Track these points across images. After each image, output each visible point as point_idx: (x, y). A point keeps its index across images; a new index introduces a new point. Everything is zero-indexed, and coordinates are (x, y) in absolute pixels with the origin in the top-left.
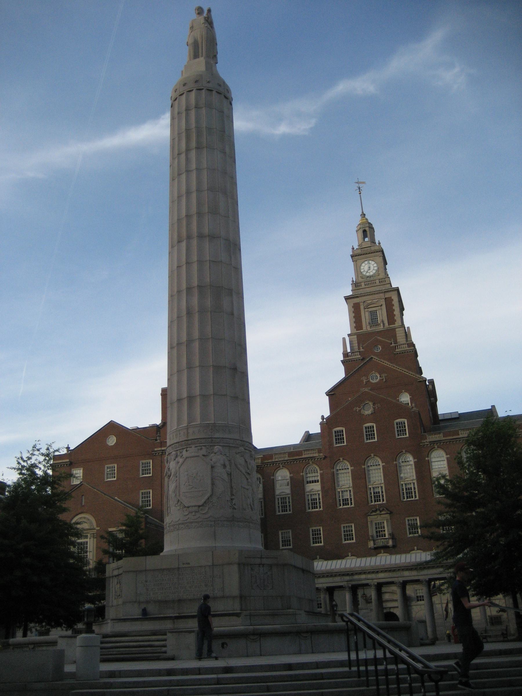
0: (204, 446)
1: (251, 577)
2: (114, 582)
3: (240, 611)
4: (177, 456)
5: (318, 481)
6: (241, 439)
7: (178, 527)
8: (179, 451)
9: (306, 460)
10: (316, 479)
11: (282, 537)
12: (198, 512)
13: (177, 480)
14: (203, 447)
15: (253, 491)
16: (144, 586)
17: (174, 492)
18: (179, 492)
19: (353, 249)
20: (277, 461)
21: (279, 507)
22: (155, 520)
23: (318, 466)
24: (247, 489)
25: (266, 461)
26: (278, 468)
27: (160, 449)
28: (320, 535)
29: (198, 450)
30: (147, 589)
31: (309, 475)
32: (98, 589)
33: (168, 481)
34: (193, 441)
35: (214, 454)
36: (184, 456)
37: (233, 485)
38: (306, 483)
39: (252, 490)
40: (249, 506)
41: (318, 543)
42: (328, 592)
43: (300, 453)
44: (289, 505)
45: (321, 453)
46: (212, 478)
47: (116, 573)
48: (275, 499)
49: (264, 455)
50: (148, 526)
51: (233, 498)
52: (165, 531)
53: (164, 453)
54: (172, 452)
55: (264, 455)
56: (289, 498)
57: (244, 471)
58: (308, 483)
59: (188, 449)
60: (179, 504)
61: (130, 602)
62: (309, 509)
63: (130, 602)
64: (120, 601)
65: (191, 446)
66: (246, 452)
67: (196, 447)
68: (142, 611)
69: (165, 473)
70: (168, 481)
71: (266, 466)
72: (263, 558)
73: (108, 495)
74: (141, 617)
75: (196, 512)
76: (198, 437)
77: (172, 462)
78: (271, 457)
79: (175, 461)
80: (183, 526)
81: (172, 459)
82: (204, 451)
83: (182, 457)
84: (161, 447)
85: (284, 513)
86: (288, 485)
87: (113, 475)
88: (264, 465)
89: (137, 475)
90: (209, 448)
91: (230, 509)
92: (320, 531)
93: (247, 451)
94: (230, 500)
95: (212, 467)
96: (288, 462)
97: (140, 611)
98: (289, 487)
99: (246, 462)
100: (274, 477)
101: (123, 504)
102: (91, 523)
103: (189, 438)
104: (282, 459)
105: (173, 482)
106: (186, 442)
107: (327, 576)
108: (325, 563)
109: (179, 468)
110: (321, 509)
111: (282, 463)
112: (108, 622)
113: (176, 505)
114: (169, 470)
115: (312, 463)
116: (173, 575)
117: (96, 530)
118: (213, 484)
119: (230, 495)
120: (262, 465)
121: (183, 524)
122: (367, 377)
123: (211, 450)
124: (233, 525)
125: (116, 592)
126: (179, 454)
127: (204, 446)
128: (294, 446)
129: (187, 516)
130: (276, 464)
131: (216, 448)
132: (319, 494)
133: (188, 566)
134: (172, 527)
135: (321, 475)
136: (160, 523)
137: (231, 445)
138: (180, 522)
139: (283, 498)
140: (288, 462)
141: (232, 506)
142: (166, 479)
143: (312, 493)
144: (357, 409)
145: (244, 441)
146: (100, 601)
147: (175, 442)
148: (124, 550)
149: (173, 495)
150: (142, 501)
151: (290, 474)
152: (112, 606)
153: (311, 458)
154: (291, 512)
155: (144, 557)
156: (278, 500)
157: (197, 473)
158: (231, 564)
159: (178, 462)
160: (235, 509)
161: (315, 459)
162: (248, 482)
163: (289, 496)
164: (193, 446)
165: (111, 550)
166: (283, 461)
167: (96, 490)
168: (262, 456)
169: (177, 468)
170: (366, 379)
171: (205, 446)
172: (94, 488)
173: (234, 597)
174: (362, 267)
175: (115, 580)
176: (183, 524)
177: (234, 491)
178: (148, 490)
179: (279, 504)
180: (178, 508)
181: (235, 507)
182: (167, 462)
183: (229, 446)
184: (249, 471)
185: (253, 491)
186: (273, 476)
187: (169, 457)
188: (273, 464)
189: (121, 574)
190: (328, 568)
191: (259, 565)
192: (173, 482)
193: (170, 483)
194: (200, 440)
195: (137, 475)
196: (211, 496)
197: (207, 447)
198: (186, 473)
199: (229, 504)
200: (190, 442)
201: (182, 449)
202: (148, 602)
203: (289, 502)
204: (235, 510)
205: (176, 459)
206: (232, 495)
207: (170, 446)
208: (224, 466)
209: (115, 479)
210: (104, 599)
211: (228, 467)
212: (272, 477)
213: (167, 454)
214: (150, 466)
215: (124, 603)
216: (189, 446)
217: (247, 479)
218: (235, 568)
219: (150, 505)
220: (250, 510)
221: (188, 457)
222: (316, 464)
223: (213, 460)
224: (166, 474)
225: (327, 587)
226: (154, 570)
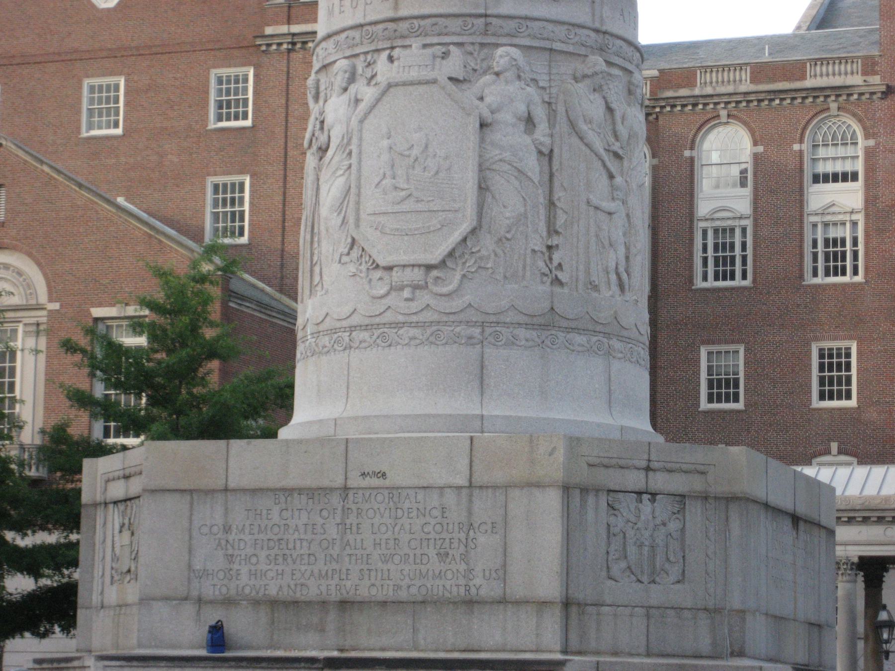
0: (454, 44)
1: (608, 537)
2: (109, 525)
3: (559, 656)
4: (352, 78)
5: (854, 177)
6: (597, 25)
7: (347, 339)
8: (362, 58)
9: (815, 97)
10: (848, 167)
11: (710, 368)
12: (426, 287)
13: (350, 167)
14: (452, 48)
15: (629, 222)
16: (219, 544)
17: (340, 206)
18: (358, 210)
20: (711, 96)
21: (705, 260)
22: (261, 285)
23: (860, 121)
24: (610, 214)
25: (670, 94)
26: (710, 121)
27: (284, 29)
28: (848, 368)
29: (434, 57)
30: (230, 558)
31: (822, 152)
32: (50, 526)
33: (318, 169)
34: (415, 21)
35: (494, 77)
36: (379, 78)
37: (556, 197)
38: (811, 179)
39: (628, 215)
40: (613, 277)
41: (840, 398)
42: (862, 573)
43: (797, 70)
44: (744, 259)
45: (874, 73)
46: (480, 165)
47: (117, 490)
49: (660, 71)
50: (232, 304)
51: (555, 242)
52: (300, 349)
53: (299, 46)
54: (335, 62)
55: (660, 71)
56: (744, 230)
57: (599, 146)
58: (818, 182)
59: (396, 53)
60: (355, 253)
61: (166, 599)
62: (815, 274)
63: (166, 599)
64: (132, 593)
66: (610, 75)
67: (425, 46)
68: (210, 632)
69: (308, 135)
70: (318, 169)
71: (668, 109)
72: (654, 470)
73: (89, 190)
74: (203, 653)
75: (415, 287)
76: (435, 11)
77: (334, 95)
78: (687, 77)
79: (345, 97)
80: (365, 335)
81: (336, 88)
82: (454, 64)
83: (373, 82)
84: (289, 23)
85: (721, 284)
86: (743, 184)
87: (112, 118)
88: (662, 107)
89: (197, 122)
90: (476, 54)
91: (543, 283)
92: (848, 355)
93: (616, 71)
94: (544, 250)
95: (483, 125)
96: (749, 102)
97: (202, 634)
98: (748, 191)
99: (610, 110)
100: (694, 153)
101: (146, 224)
102: (29, 286)
103: (403, 13)
104: (730, 89)
105: (334, 172)
106: (391, 26)
107: (866, 520)
108: (861, 471)
109: (361, 121)
110: (859, 278)
111: (727, 103)
112: (87, 663)
113: (345, 259)
114: (322, 128)
115: (839, 109)
116: (325, 513)
117: (44, 313)
118: (483, 188)
119: (545, 234)
120: (654, 107)
121: (366, 327)
123: (483, 60)
124: (548, 342)
125: (115, 558)
126: (360, 70)
127: (454, 44)
128: (778, 43)
129: (383, 301)
130: (705, 105)
131: (502, 56)
132: (854, 224)
133: (376, 482)
134: (327, 338)
135: (870, 154)
136: (278, 295)
137: (557, 46)
138: (356, 320)
139: (724, 230)
140: (749, 102)
141: (547, 271)
142: (311, 160)
143: (828, 218)
145: (605, 33)
146: (58, 568)
147: (350, 22)
148: (147, 395)
149: (336, 221)
150: (216, 216)
151: (755, 144)
152: (102, 607)
153: (837, 90)
154: (747, 283)
155: (222, 443)
157: (426, 147)
158: (538, 485)
159: (357, 101)
160: (561, 284)
161: (852, 95)
162: (613, 188)
163: (744, 222)
164: (416, 43)
165: (99, 390)
166: (730, 94)
167: (46, 169)
168: (655, 73)
169: (354, 122)
171: (460, 45)
172: (42, 162)
173: (542, 605)
175: (115, 517)
176: (366, 327)
177: (561, 219)
178: (236, 178)
179: (705, 249)
180: (352, 268)
181: (560, 275)
182: (317, 98)
183: (551, 50)
184: (618, 144)
185: (629, 222)
186: (692, 148)
187: (323, 79)
188: (695, 105)
189: (139, 497)
190: (871, 491)
191: (639, 493)
192: (334, 172)
193: (324, 175)
194: (441, 21)
195: (197, 122)
196: (473, 231)
197: (470, 48)
198: (385, 143)
199: (541, 264)
200: (403, 26)
202: (229, 602)
203: (744, 247)
204: (557, 289)
205: (353, 89)
206: (552, 231)
207: (329, 36)
208: (529, 122)
209: (119, 131)
210: (74, 563)
211: (542, 128)
212: (687, 153)
213: (316, 66)
214: (245, 90)
215: (145, 601)
216: (399, 42)
217: (611, 177)
218: (552, 500)
219: (242, 229)
220: (615, 288)
221: (397, 85)
222: (854, 115)
223: (488, 100)
224: (311, 141)
225: (861, 558)
226: (255, 492)
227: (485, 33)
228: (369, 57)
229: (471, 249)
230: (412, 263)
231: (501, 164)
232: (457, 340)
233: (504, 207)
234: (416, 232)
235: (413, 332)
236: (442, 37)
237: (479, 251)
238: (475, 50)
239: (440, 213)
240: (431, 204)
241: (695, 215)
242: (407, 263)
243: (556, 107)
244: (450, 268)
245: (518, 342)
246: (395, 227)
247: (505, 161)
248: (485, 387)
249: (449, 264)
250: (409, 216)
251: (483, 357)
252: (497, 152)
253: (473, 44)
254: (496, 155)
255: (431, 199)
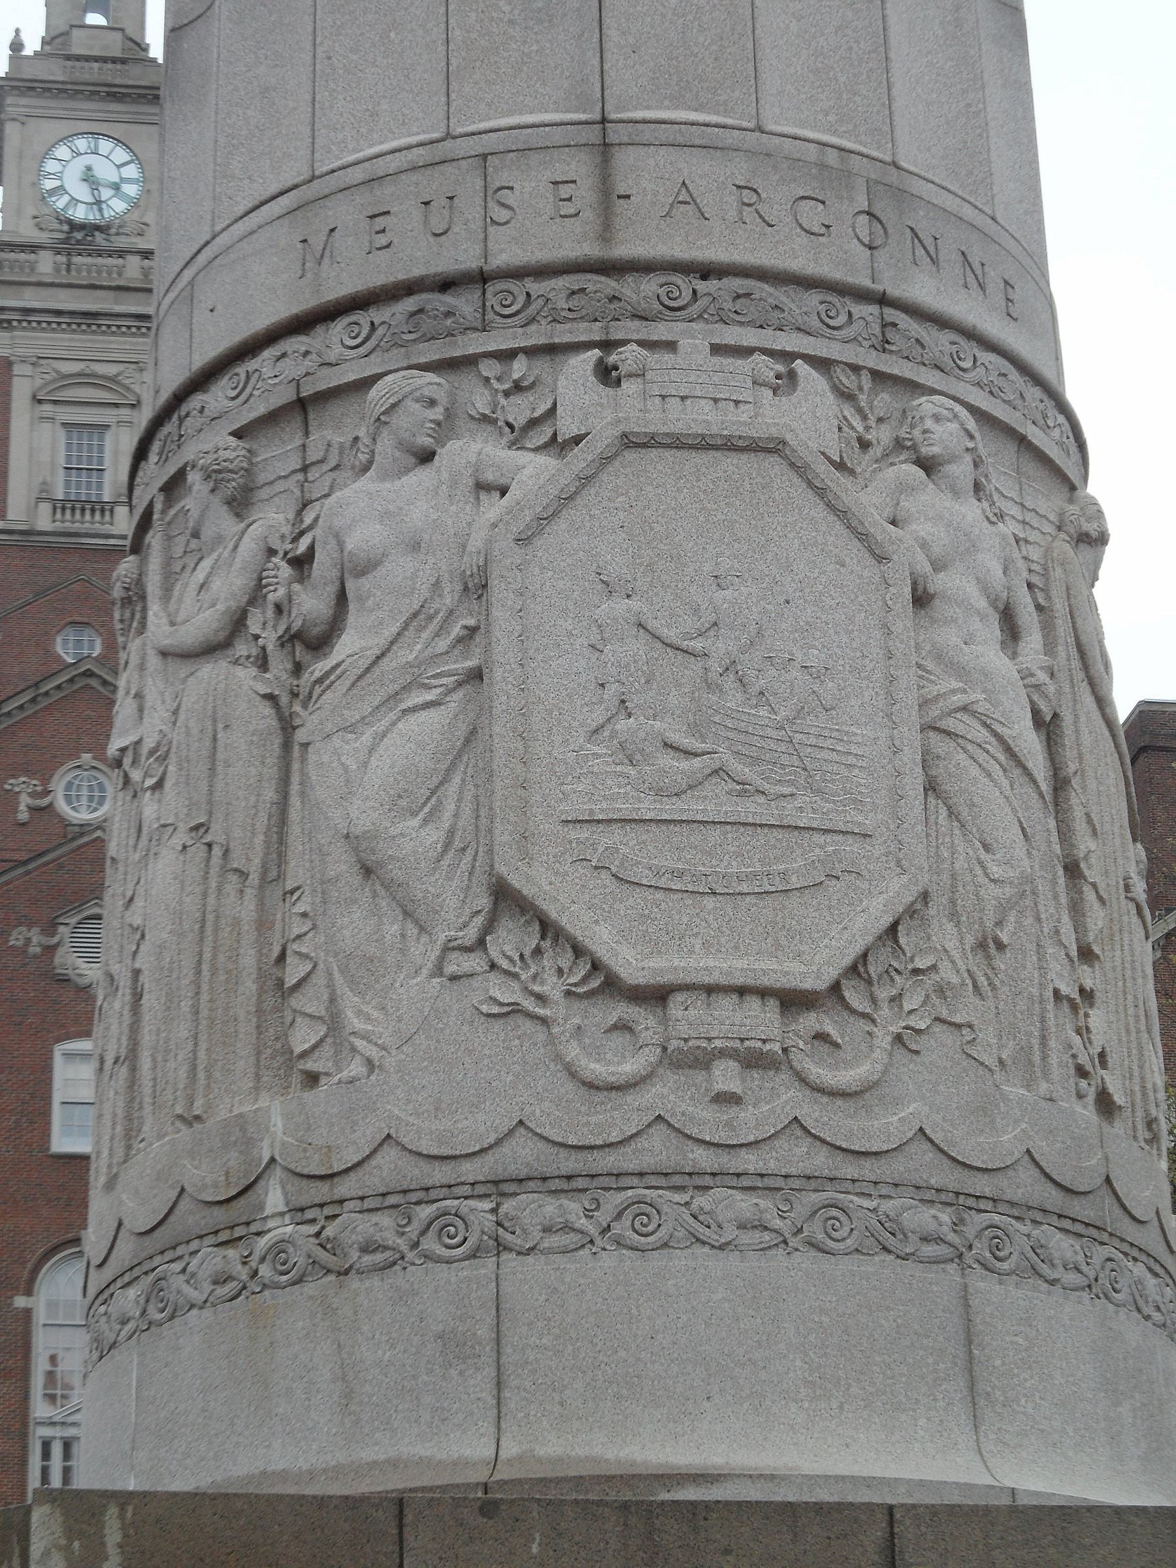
19: (16, 46)
48: (25, 1447)
65: (660, 331)
122: (45, 781)
144: (28, 940)
156: (46, 1455)
170: (33, 795)
171: (822, 364)
174: (51, 166)
197: (847, 380)
201: (531, 352)
211: (1033, 641)
227: (883, 345)
228: (519, 368)
229: (912, 960)
230: (740, 981)
231: (965, 717)
232: (891, 1242)
233: (987, 847)
234: (745, 888)
235: (745, 1204)
236: (769, 332)
237: (934, 968)
238: (861, 389)
239: (819, 839)
240: (789, 806)
241: (32, 1416)
242: (723, 981)
243: (1048, 598)
244: (853, 1012)
245: (1045, 1269)
246: (671, 864)
247: (974, 714)
248: (982, 1402)
249: (854, 996)
250: (715, 835)
251: (967, 1306)
252: (955, 684)
253: (856, 369)
254: (954, 692)
255: (787, 790)
